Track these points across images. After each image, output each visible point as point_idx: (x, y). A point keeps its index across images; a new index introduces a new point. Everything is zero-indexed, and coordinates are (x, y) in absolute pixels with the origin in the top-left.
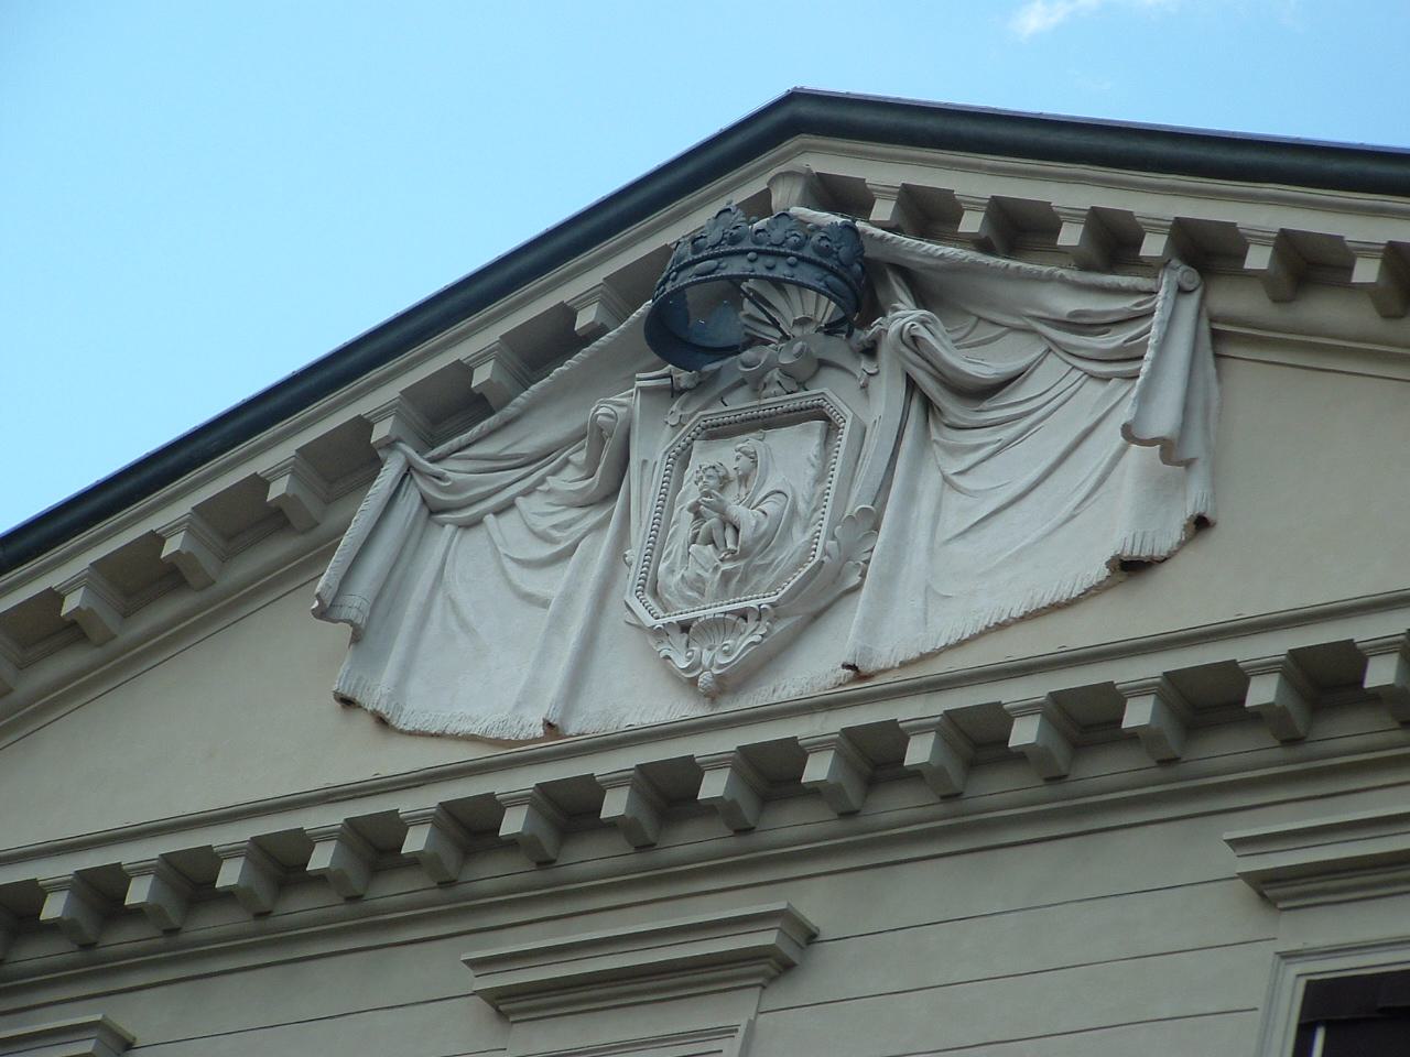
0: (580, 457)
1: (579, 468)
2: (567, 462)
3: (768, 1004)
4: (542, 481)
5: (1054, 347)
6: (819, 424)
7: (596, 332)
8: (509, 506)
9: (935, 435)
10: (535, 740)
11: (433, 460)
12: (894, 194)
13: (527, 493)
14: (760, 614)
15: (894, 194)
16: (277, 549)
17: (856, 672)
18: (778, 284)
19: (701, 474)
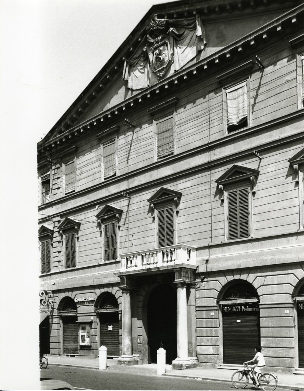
0: (143, 56)
1: (143, 57)
2: (141, 57)
3: (177, 107)
4: (140, 59)
5: (187, 29)
6: (165, 45)
7: (141, 40)
8: (137, 63)
9: (177, 42)
10: (147, 87)
11: (129, 60)
12: (130, 220)
13: (139, 61)
14: (165, 67)
15: (130, 220)
16: (95, 100)
17: (176, 71)
18: (71, 168)
19: (86, 300)
